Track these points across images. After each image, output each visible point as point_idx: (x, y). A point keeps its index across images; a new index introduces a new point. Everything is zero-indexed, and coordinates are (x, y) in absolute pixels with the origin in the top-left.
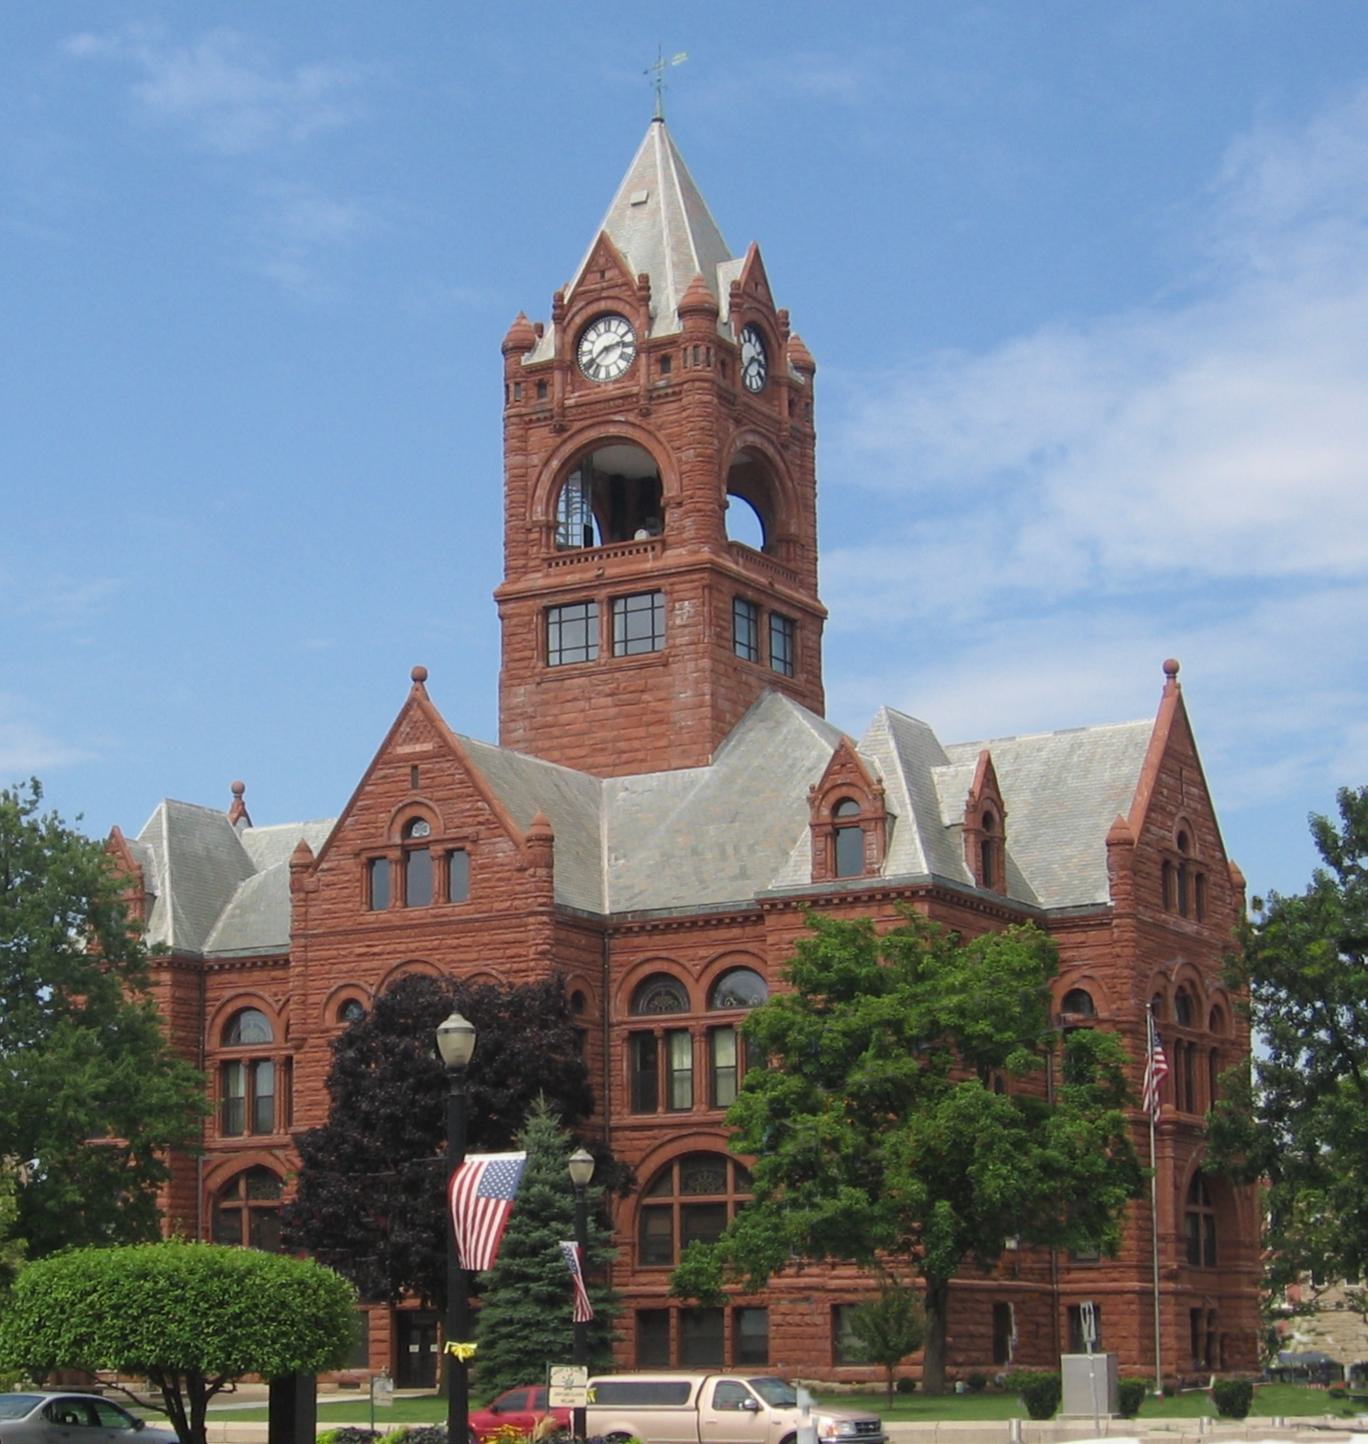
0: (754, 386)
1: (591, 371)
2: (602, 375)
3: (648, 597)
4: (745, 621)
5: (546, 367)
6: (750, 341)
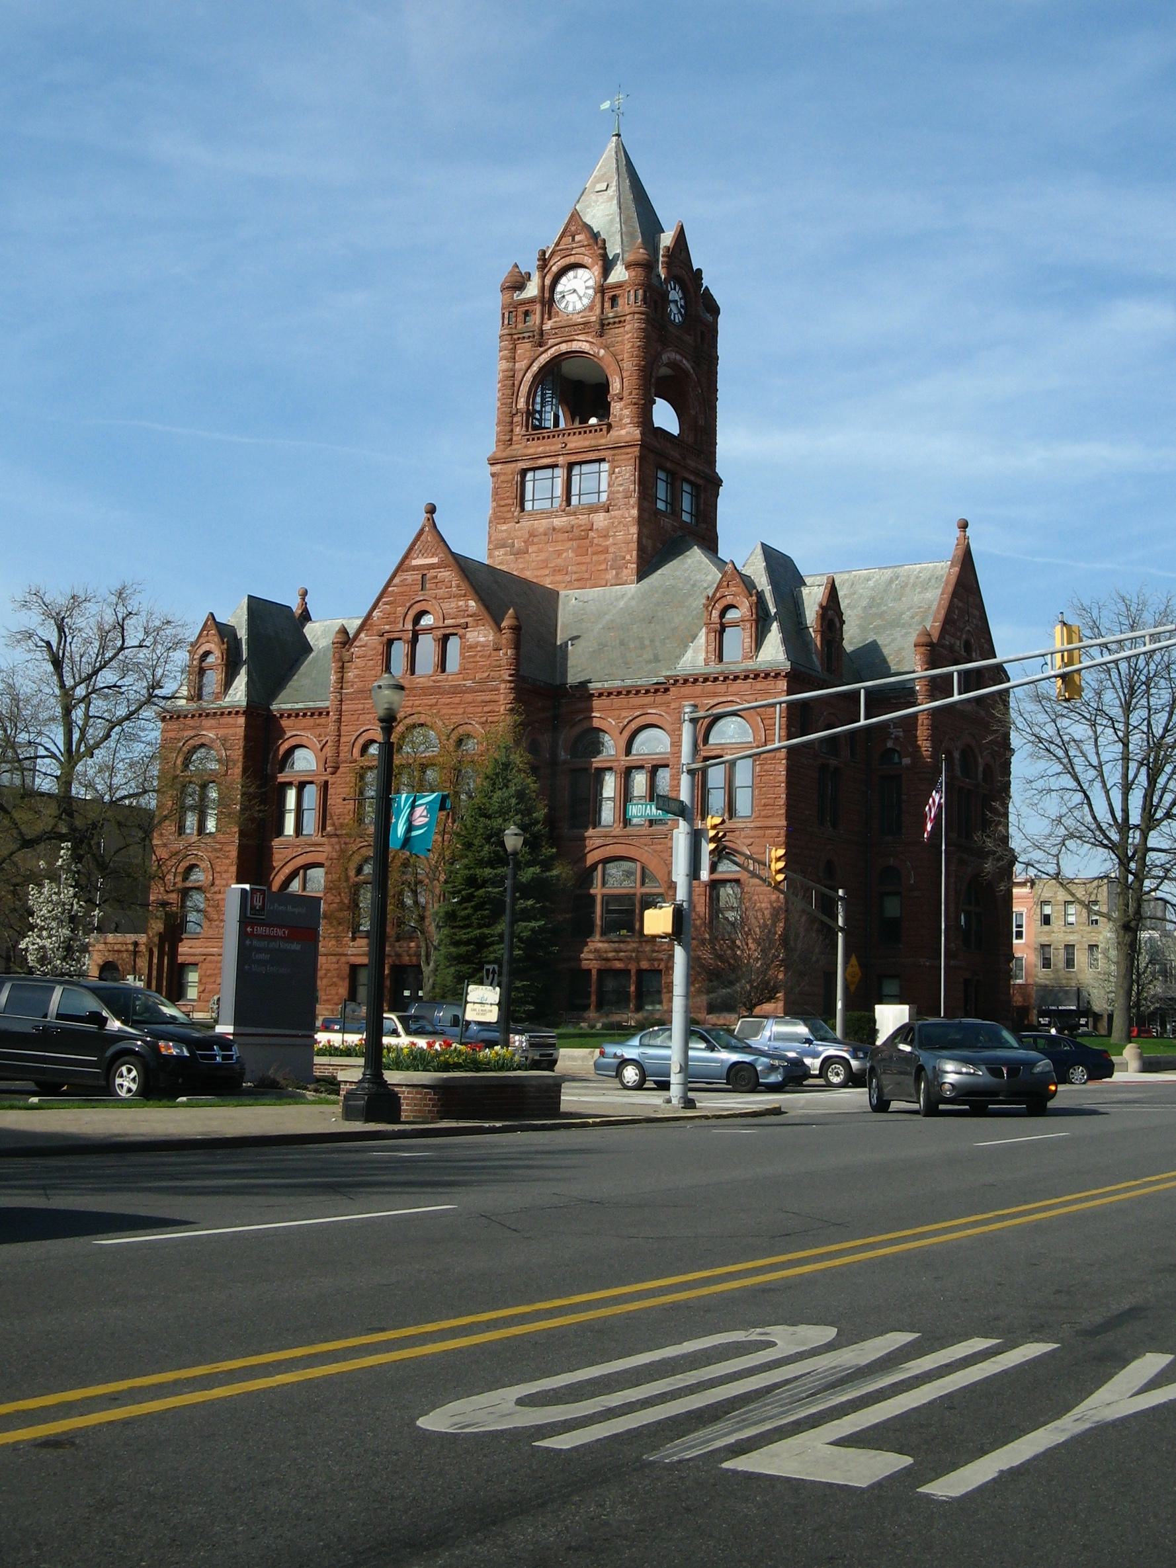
0: (677, 321)
1: (563, 305)
2: (570, 309)
3: (597, 465)
4: (690, 496)
5: (531, 301)
6: (675, 289)
